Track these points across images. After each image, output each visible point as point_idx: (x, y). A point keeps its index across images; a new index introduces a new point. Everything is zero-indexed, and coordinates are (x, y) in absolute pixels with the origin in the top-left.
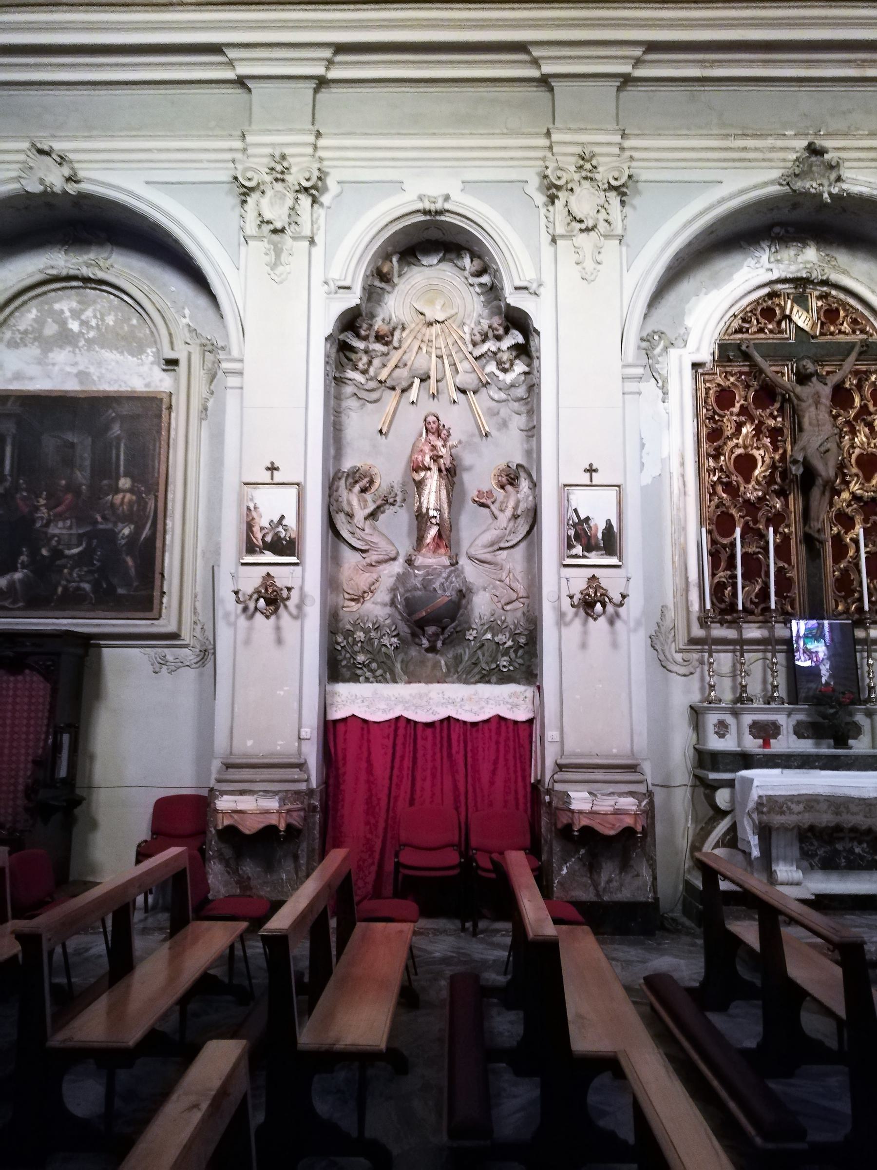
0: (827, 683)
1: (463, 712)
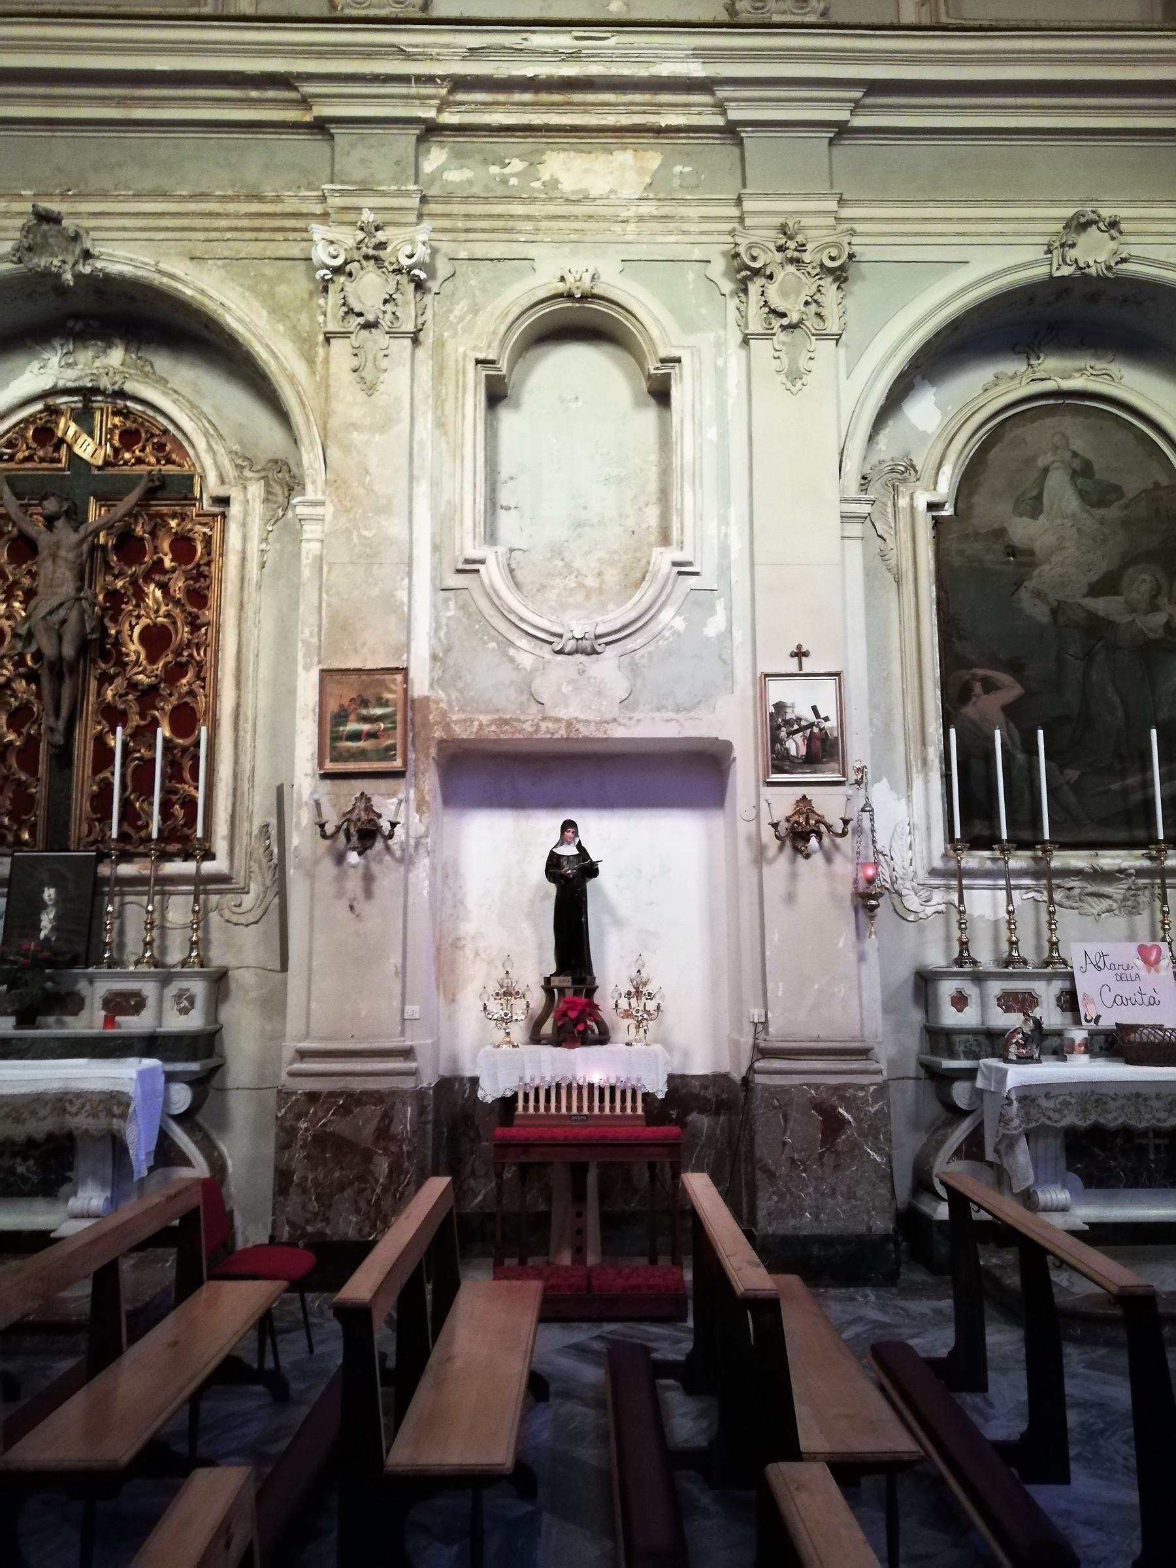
0: (47, 938)
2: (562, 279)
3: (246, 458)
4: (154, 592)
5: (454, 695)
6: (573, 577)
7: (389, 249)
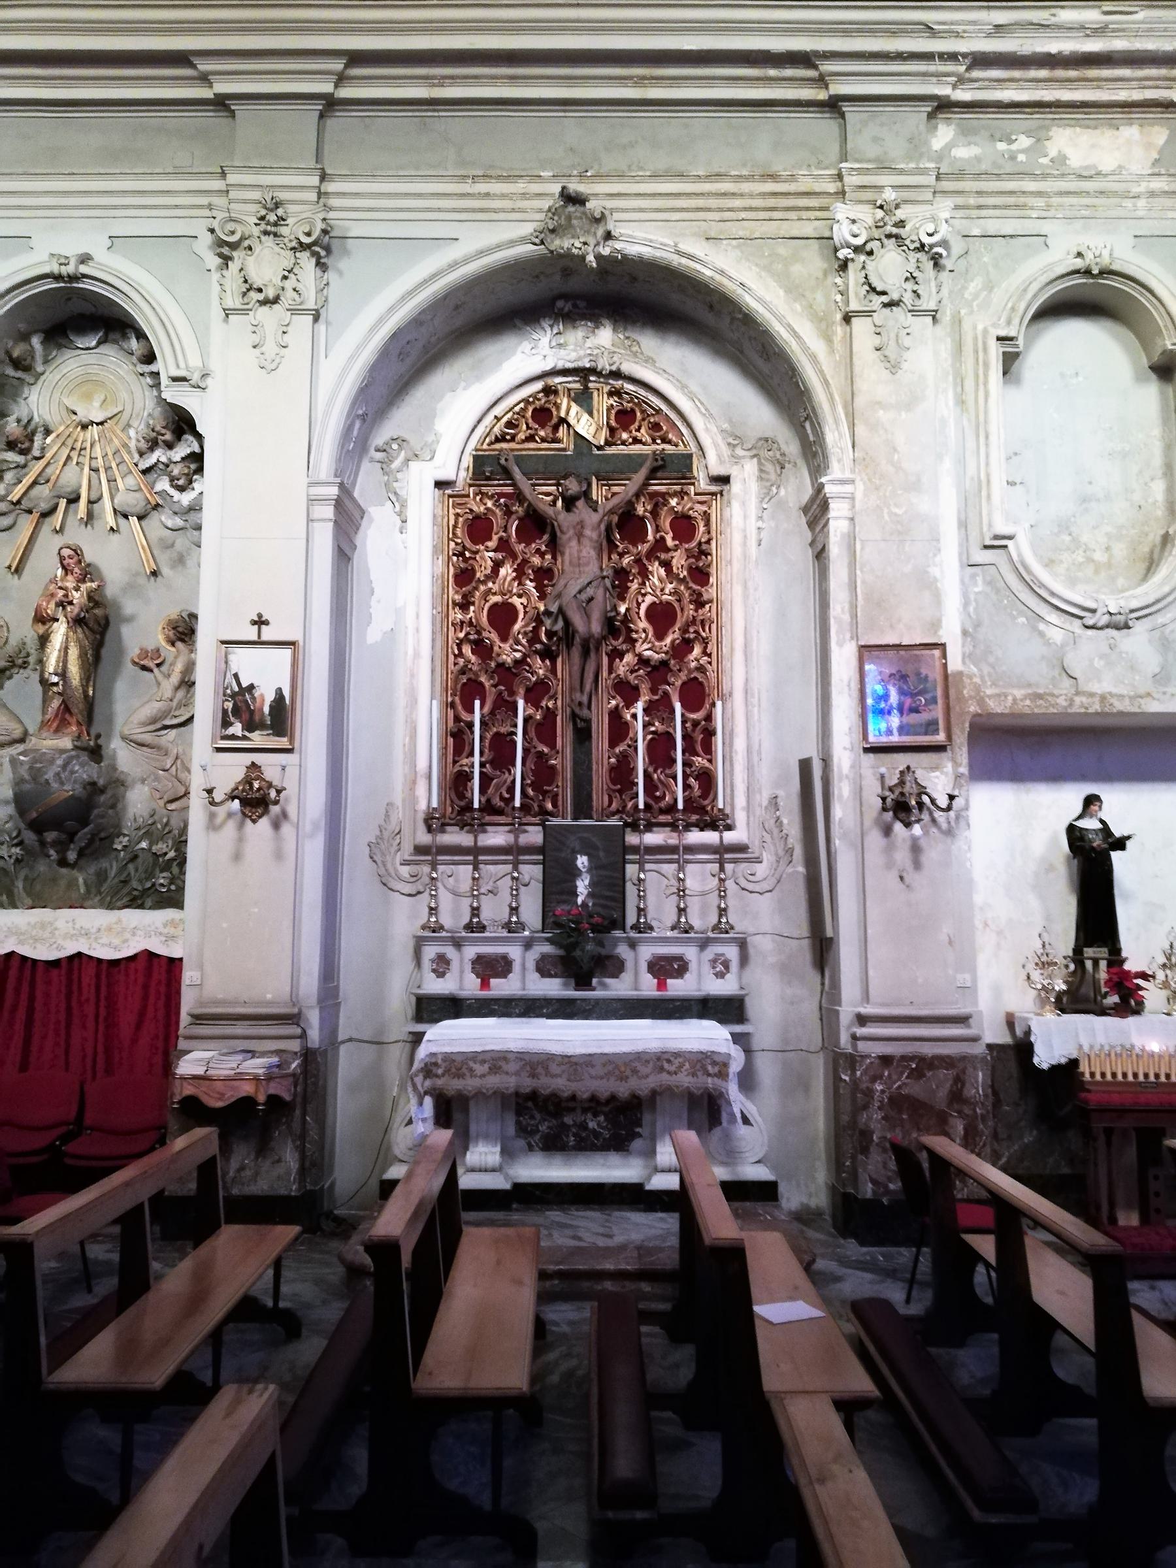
0: (584, 904)
1: (98, 946)
2: (1079, 255)
3: (736, 437)
4: (657, 571)
5: (986, 670)
6: (1081, 552)
7: (908, 228)
